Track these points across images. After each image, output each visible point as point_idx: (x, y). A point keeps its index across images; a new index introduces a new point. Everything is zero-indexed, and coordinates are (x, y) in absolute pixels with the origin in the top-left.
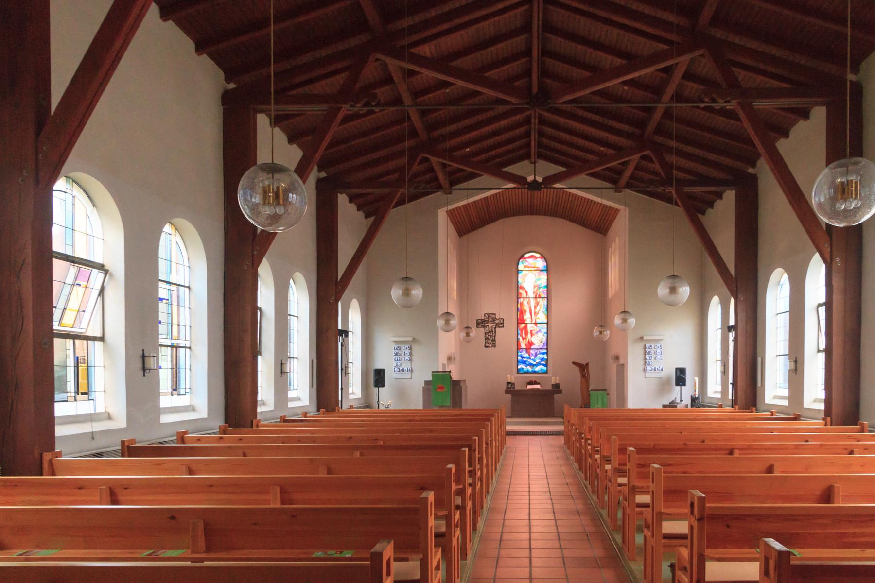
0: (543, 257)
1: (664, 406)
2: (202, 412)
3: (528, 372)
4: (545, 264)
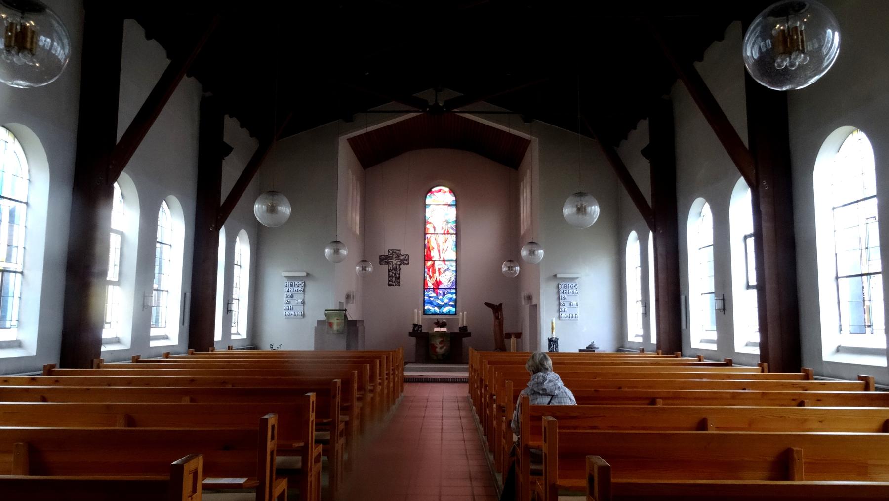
0: (451, 191)
1: (580, 351)
2: (31, 349)
4: (454, 198)
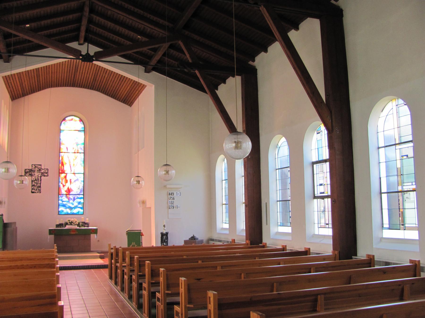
3: (68, 214)
4: (83, 126)
